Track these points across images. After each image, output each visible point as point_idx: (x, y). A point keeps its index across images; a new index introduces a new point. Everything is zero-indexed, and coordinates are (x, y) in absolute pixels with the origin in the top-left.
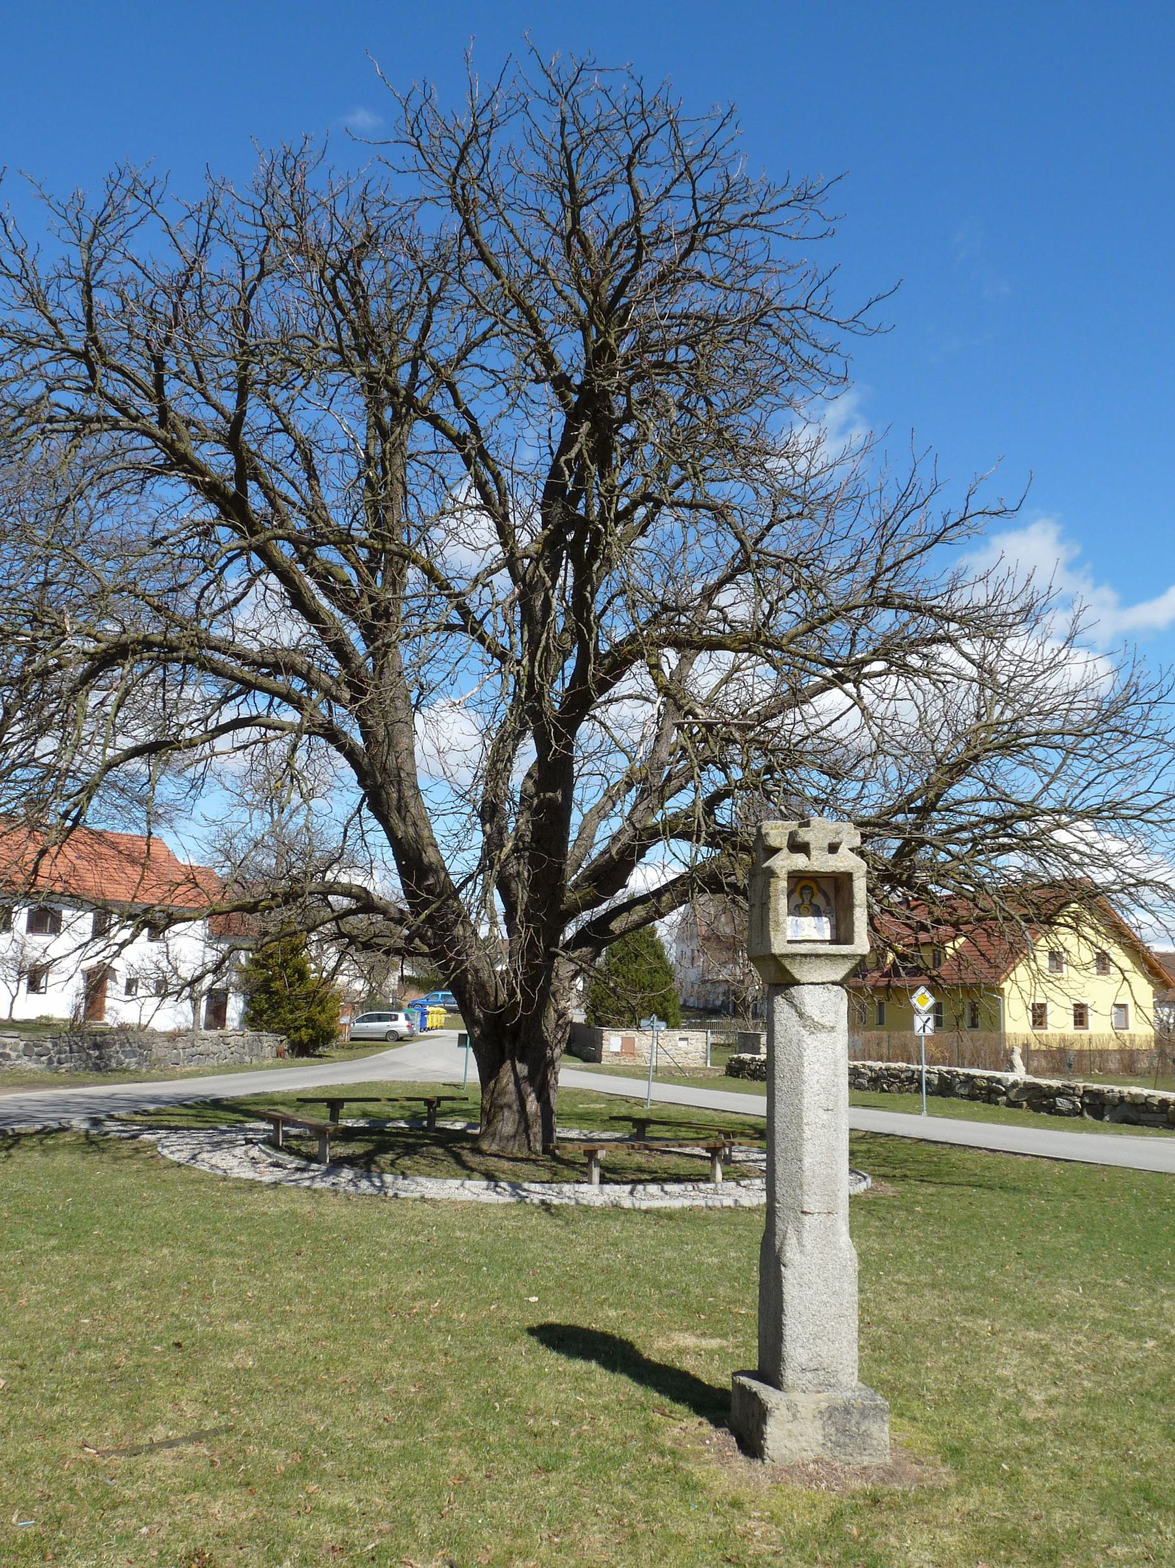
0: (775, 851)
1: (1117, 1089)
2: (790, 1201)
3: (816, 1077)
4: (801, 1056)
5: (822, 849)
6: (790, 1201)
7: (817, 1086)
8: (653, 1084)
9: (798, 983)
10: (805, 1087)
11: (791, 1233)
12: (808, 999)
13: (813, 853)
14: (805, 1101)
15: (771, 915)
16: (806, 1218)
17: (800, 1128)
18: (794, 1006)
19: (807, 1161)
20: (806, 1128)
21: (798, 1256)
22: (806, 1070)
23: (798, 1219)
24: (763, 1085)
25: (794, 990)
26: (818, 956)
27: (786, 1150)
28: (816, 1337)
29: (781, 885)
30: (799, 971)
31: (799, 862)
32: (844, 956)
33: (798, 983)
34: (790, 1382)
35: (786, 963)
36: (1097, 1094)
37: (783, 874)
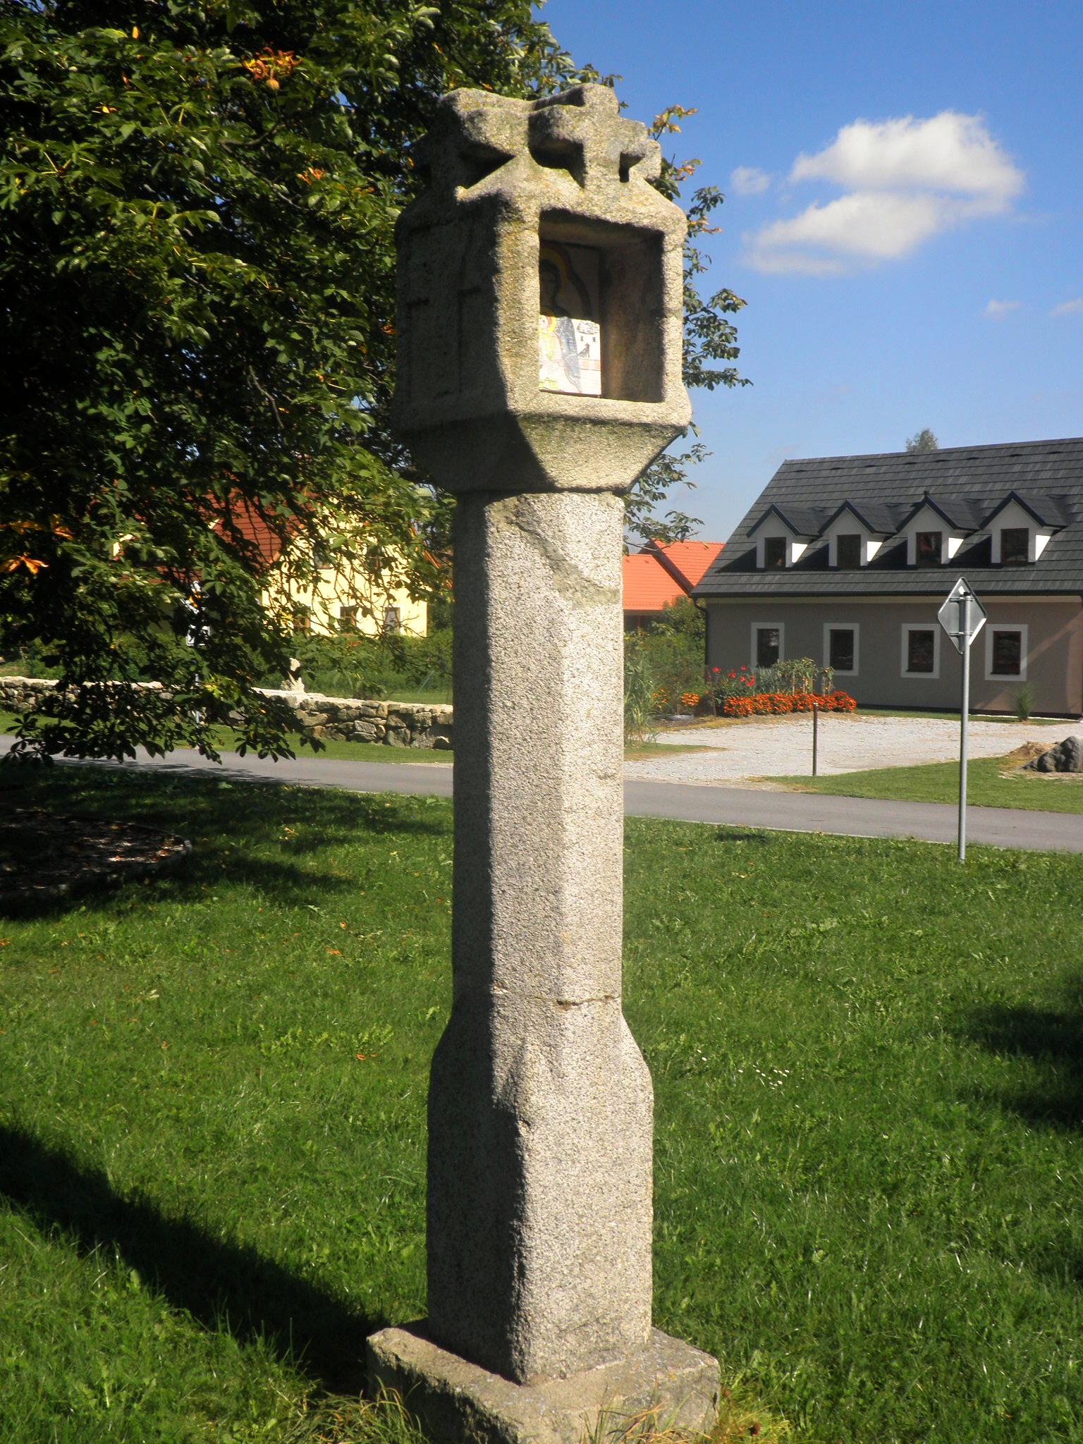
0: (498, 159)
1: (428, 707)
2: (531, 981)
3: (584, 705)
4: (555, 658)
5: (606, 164)
6: (531, 981)
7: (587, 726)
8: (973, 727)
9: (550, 487)
10: (566, 728)
11: (533, 1052)
12: (571, 526)
13: (593, 171)
14: (567, 759)
15: (503, 315)
16: (569, 1016)
17: (554, 819)
18: (539, 541)
19: (570, 891)
20: (567, 819)
21: (552, 1099)
22: (568, 690)
23: (549, 1019)
24: (959, 716)
25: (540, 503)
26: (598, 422)
27: (521, 870)
28: (586, 1258)
29: (521, 245)
30: (559, 460)
31: (559, 188)
32: (646, 427)
33: (550, 487)
34: (538, 1366)
35: (534, 436)
36: (406, 716)
37: (531, 215)
